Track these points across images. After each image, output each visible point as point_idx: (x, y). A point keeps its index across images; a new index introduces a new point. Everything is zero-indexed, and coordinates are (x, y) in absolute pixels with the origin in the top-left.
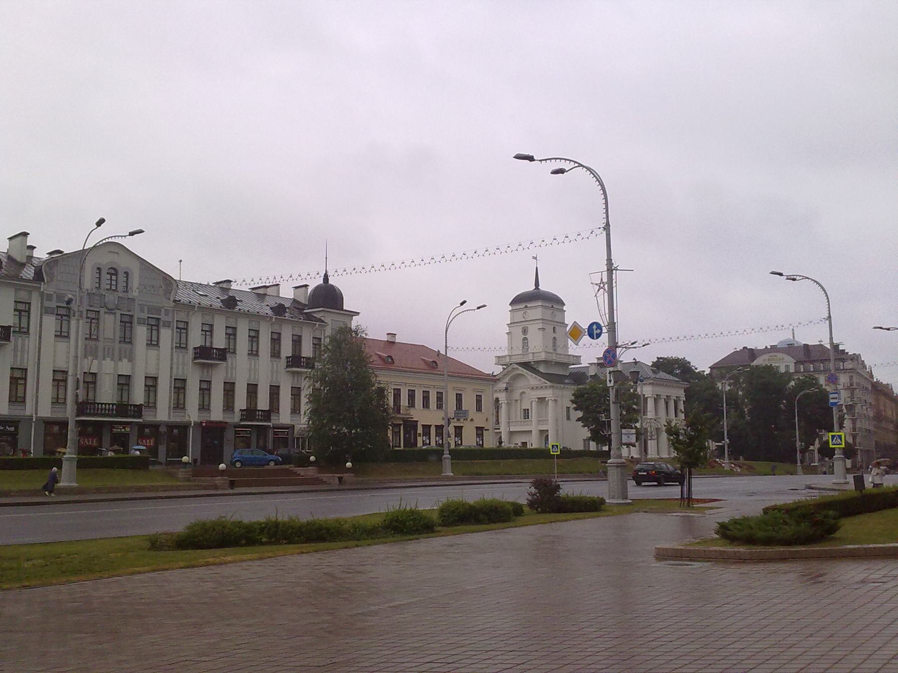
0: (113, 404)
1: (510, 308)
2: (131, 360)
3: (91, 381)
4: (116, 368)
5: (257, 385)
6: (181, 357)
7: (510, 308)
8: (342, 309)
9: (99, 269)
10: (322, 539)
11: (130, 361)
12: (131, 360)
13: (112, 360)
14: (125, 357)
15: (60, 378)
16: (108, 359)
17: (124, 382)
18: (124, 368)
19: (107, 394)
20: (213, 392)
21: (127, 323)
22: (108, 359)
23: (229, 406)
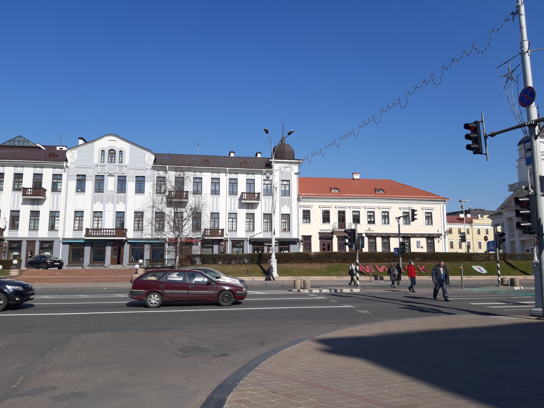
0: (113, 229)
1: (518, 148)
2: (125, 202)
3: (98, 215)
4: (115, 207)
5: (19, 211)
6: (233, 200)
7: (518, 148)
8: (156, 155)
9: (477, 151)
10: (282, 286)
11: (288, 206)
12: (125, 202)
13: (112, 203)
14: (285, 204)
15: (79, 215)
16: (110, 203)
17: (120, 216)
18: (120, 208)
19: (109, 223)
20: (84, 219)
21: (122, 182)
22: (110, 203)
23: (197, 227)
